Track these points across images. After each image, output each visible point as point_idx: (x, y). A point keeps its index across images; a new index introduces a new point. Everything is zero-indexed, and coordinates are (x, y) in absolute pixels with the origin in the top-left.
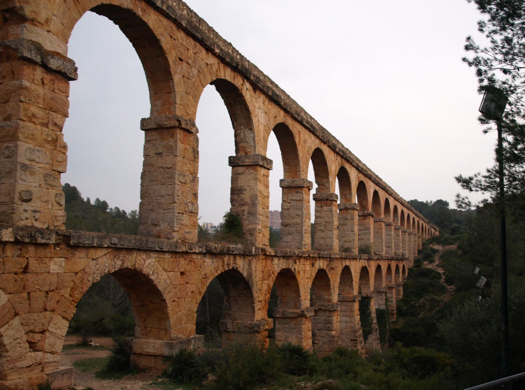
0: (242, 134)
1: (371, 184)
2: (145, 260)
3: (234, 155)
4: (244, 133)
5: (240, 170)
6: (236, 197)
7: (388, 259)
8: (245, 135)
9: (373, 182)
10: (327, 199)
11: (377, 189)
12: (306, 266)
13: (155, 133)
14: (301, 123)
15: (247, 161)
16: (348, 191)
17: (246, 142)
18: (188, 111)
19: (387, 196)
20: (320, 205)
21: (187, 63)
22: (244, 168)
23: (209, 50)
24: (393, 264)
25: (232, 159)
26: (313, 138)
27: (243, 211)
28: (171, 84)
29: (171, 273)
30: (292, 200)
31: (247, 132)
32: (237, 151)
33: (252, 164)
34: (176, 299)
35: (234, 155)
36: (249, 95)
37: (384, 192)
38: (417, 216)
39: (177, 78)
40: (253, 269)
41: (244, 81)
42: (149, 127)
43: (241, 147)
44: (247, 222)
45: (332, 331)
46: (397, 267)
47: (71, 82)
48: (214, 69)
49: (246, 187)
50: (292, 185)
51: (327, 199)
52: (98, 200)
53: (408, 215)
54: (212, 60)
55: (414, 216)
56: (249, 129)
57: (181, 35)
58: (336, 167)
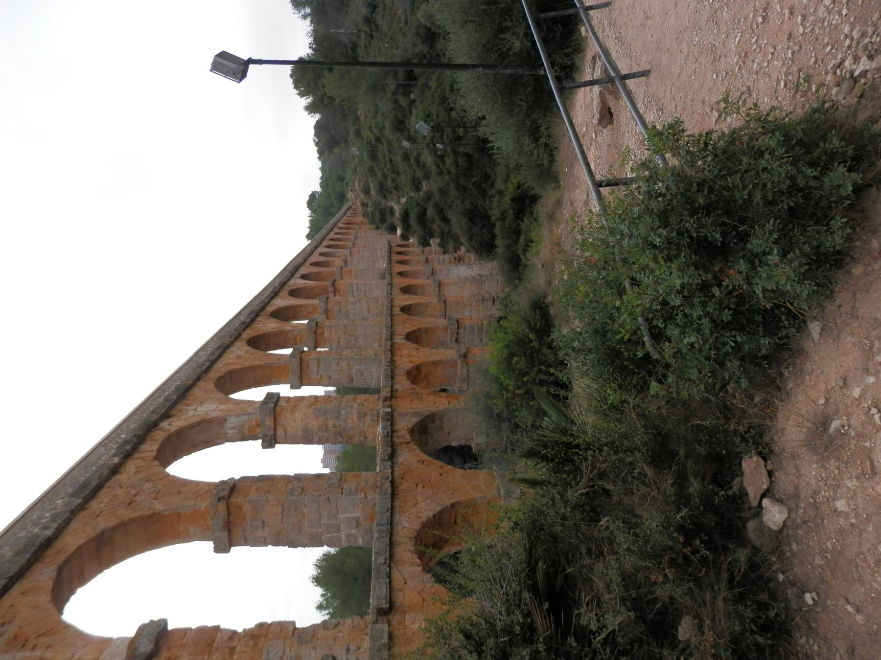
1: (292, 282)
2: (404, 528)
3: (260, 441)
7: (390, 263)
9: (289, 280)
10: (315, 332)
11: (298, 275)
14: (213, 362)
15: (269, 423)
16: (303, 309)
17: (243, 425)
18: (205, 491)
19: (308, 263)
21: (135, 495)
22: (278, 427)
23: (115, 470)
24: (395, 257)
25: (265, 444)
26: (233, 348)
27: (334, 427)
28: (167, 513)
29: (418, 498)
30: (318, 372)
32: (255, 438)
33: (273, 417)
34: (450, 492)
35: (260, 441)
36: (178, 422)
37: (302, 267)
39: (158, 506)
40: (409, 411)
41: (160, 429)
42: (227, 541)
44: (350, 421)
46: (399, 253)
47: (170, 627)
48: (142, 463)
49: (303, 424)
50: (298, 372)
51: (315, 332)
54: (131, 467)
55: (332, 233)
57: (94, 505)
58: (271, 322)
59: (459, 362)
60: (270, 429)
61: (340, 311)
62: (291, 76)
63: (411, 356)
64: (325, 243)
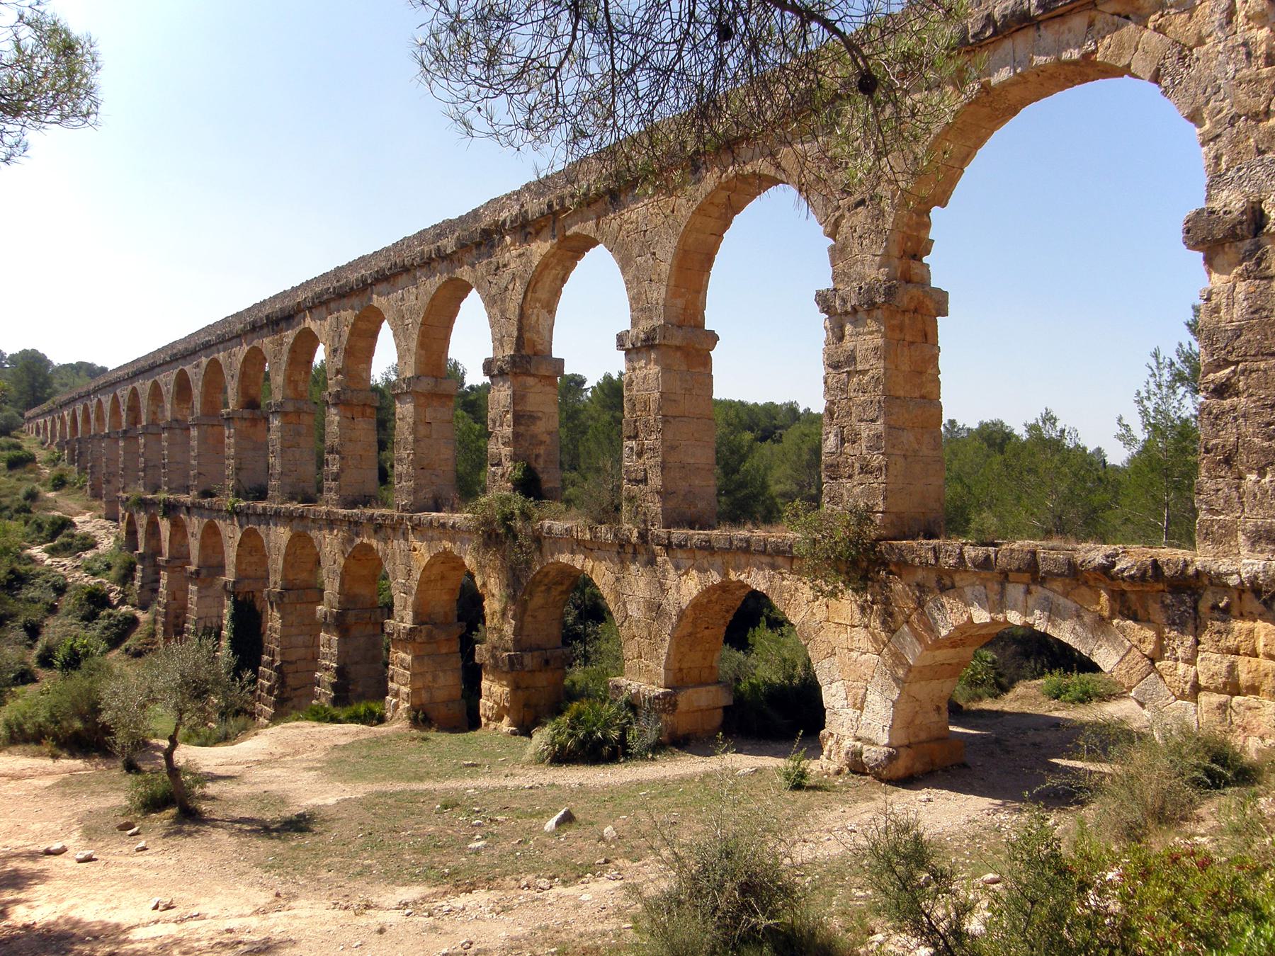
0: (534, 318)
4: (538, 316)
5: (530, 381)
6: (522, 429)
17: (538, 332)
20: (349, 415)
24: (79, 407)
25: (942, 313)
27: (537, 456)
28: (705, 278)
43: (528, 340)
49: (540, 414)
60: (537, 369)
61: (299, 434)
62: (35, 351)
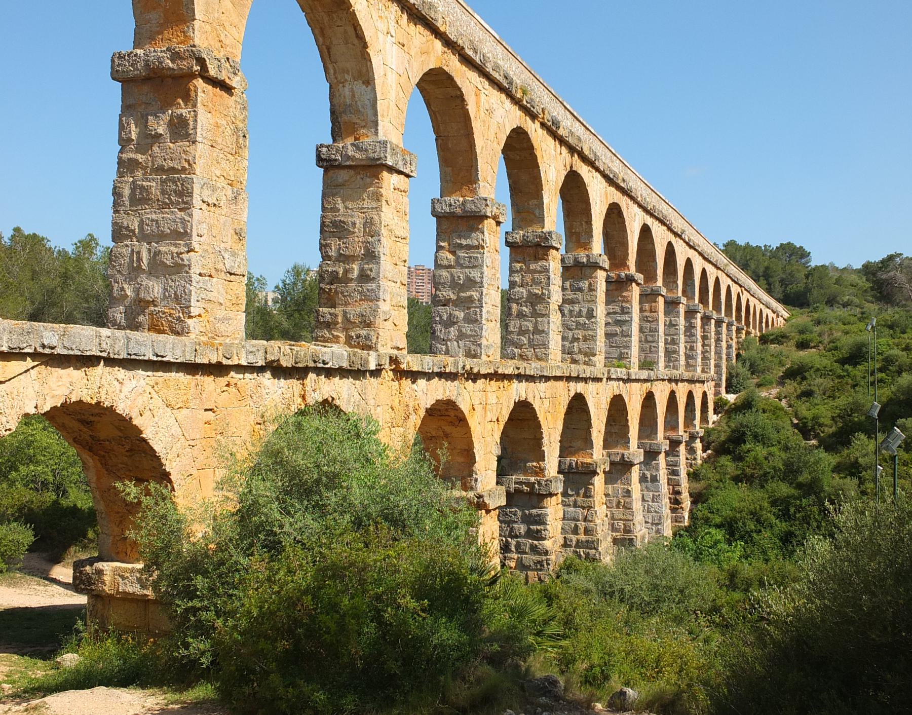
4: (352, 91)
8: (353, 96)
12: (489, 394)
13: (145, 88)
22: (352, 172)
31: (359, 87)
38: (736, 283)
45: (544, 539)
52: (17, 230)
53: (717, 280)
55: (730, 282)
56: (363, 83)
59: (471, 494)
63: (485, 408)
64: (710, 269)
